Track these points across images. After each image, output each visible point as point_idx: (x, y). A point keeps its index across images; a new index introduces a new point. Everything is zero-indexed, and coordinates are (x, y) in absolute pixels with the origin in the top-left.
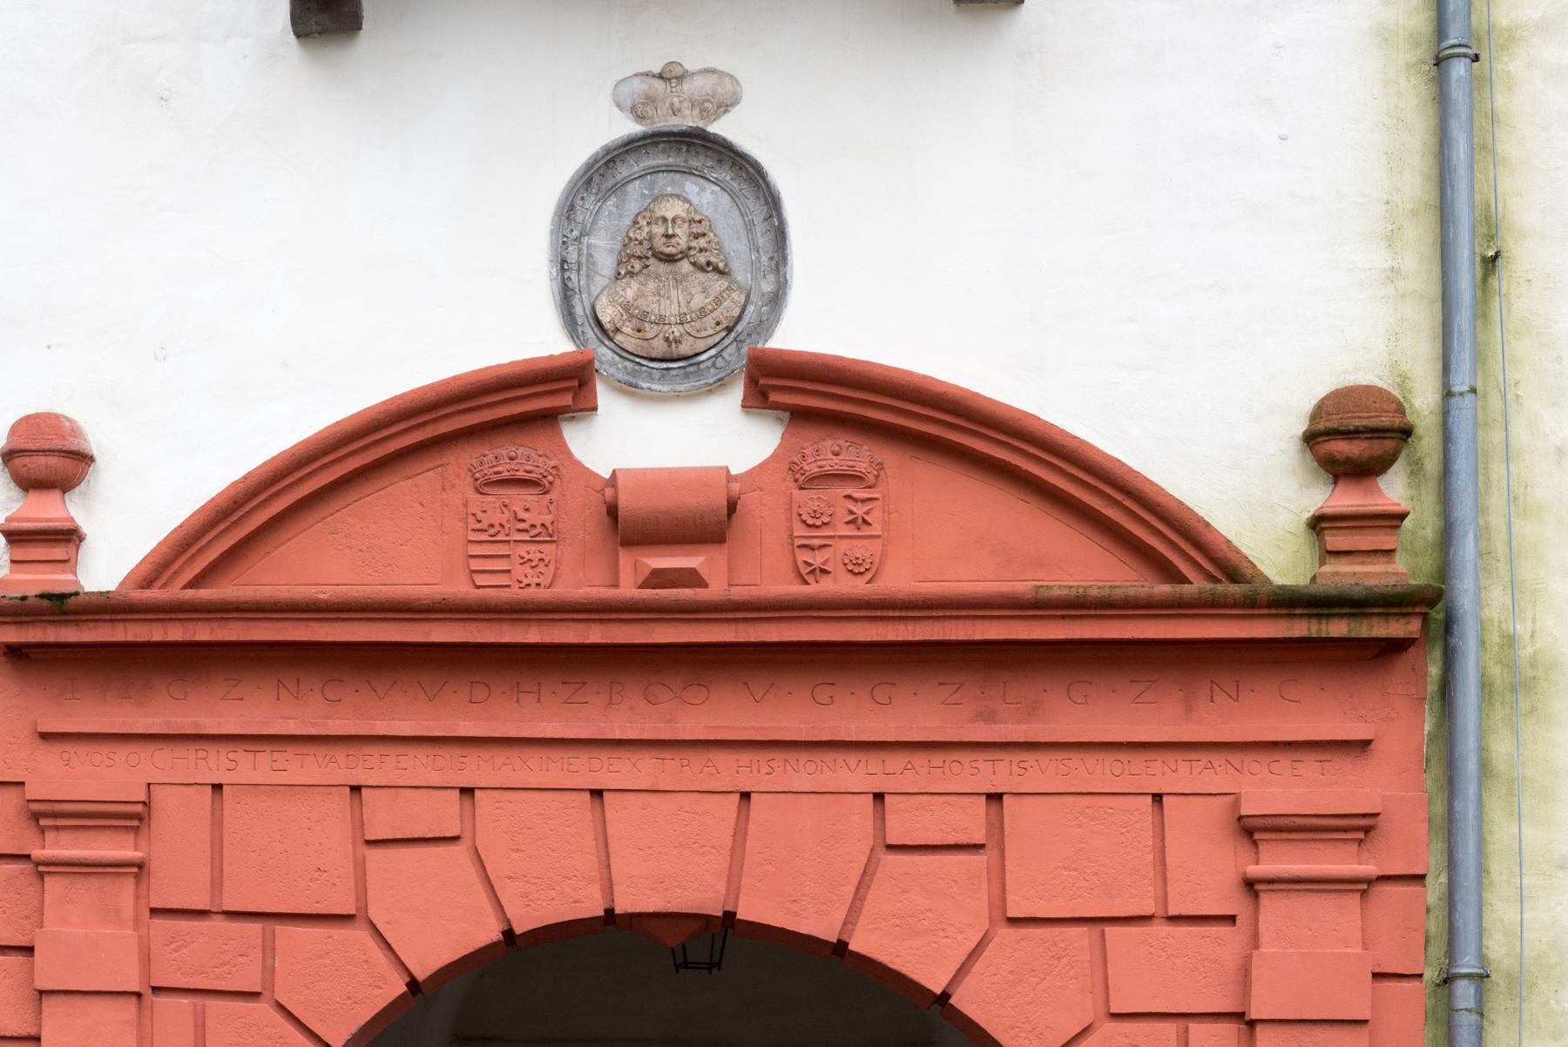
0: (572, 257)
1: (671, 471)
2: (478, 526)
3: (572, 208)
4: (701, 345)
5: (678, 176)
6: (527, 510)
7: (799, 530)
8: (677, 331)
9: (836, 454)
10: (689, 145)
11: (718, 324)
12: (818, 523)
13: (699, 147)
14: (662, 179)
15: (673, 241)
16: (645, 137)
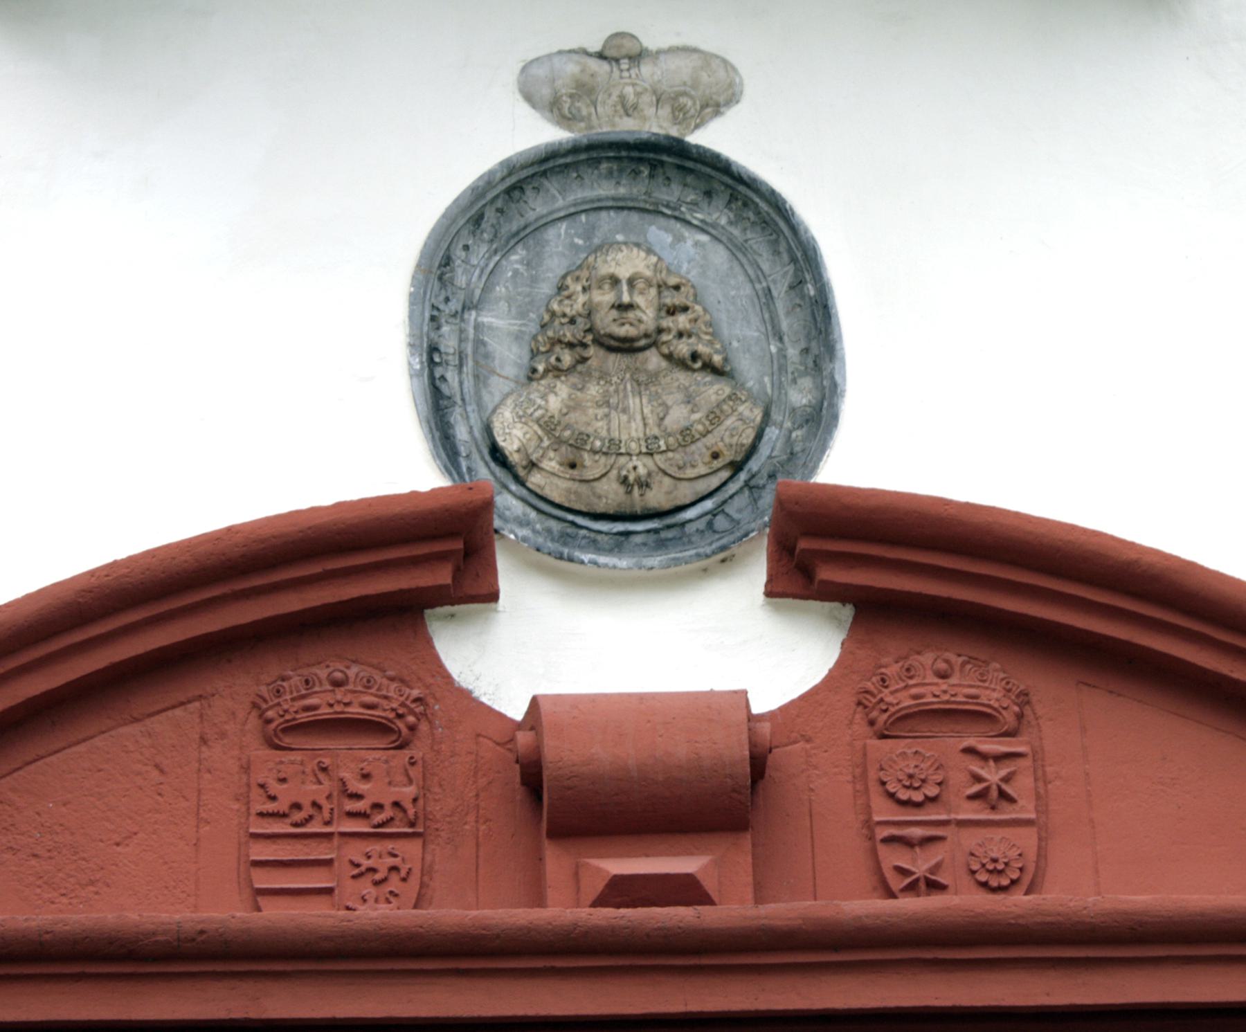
0: (449, 343)
1: (642, 698)
2: (271, 807)
3: (447, 261)
4: (685, 493)
5: (635, 217)
6: (366, 777)
7: (883, 811)
8: (642, 466)
9: (943, 676)
10: (654, 166)
11: (715, 456)
12: (918, 797)
13: (666, 168)
14: (607, 222)
15: (631, 315)
16: (575, 149)
